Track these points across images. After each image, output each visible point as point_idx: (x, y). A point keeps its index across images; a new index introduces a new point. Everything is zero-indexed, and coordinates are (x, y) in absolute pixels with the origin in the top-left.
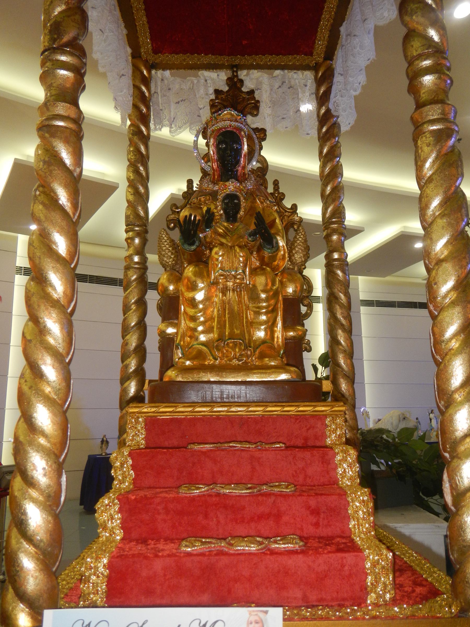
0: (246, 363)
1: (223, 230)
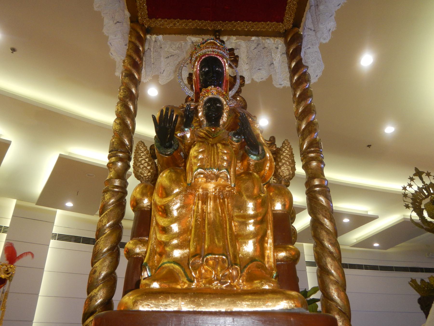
1: (205, 133)
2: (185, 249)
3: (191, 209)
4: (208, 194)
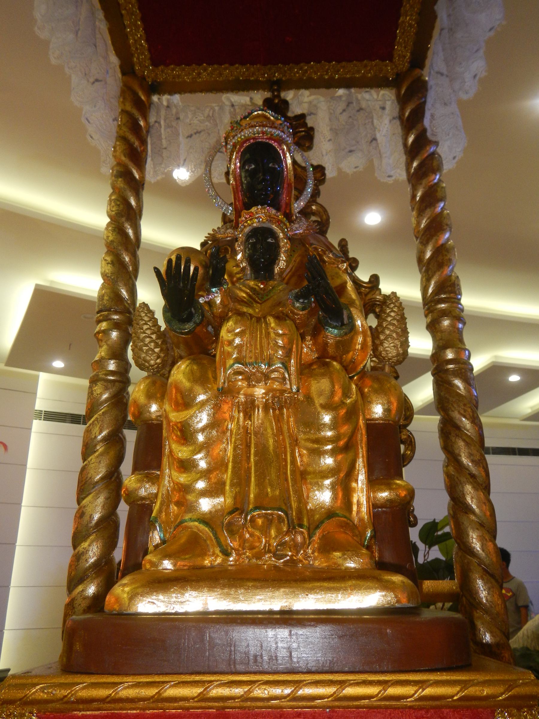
0: (293, 562)
2: (218, 497)
3: (227, 429)
4: (254, 401)
